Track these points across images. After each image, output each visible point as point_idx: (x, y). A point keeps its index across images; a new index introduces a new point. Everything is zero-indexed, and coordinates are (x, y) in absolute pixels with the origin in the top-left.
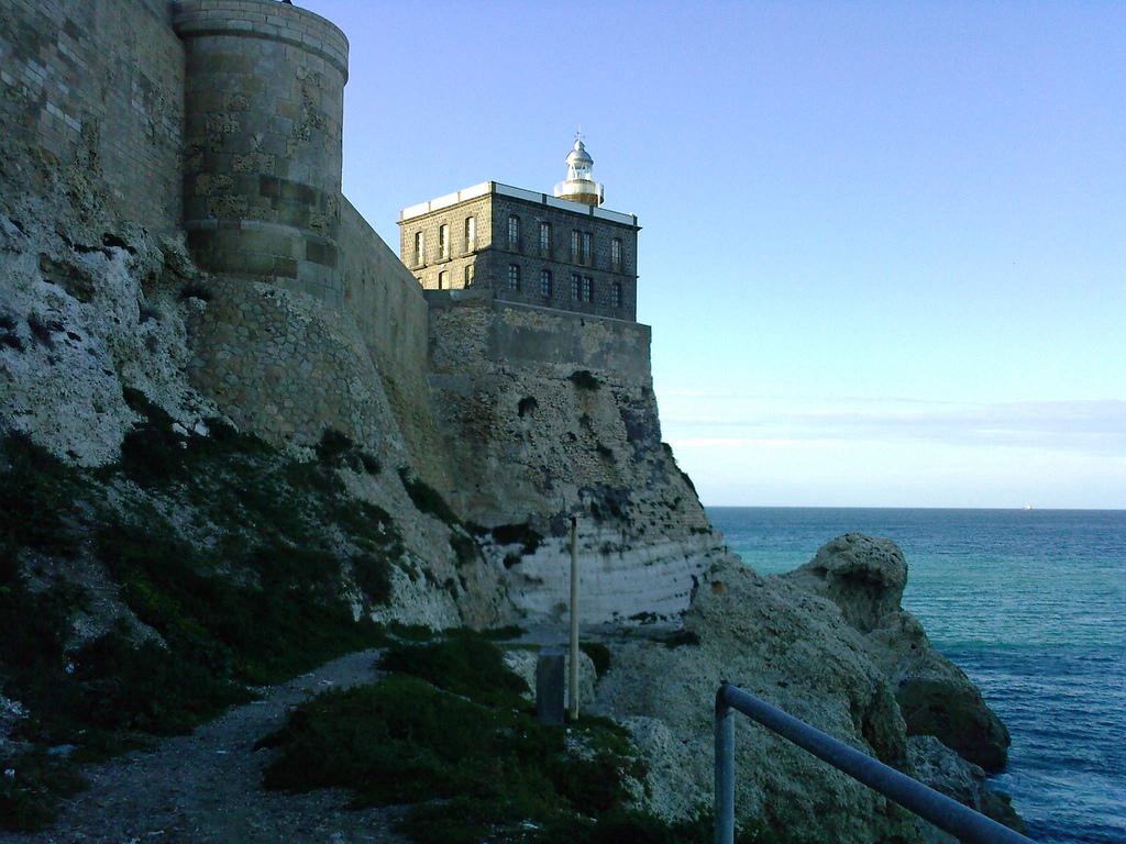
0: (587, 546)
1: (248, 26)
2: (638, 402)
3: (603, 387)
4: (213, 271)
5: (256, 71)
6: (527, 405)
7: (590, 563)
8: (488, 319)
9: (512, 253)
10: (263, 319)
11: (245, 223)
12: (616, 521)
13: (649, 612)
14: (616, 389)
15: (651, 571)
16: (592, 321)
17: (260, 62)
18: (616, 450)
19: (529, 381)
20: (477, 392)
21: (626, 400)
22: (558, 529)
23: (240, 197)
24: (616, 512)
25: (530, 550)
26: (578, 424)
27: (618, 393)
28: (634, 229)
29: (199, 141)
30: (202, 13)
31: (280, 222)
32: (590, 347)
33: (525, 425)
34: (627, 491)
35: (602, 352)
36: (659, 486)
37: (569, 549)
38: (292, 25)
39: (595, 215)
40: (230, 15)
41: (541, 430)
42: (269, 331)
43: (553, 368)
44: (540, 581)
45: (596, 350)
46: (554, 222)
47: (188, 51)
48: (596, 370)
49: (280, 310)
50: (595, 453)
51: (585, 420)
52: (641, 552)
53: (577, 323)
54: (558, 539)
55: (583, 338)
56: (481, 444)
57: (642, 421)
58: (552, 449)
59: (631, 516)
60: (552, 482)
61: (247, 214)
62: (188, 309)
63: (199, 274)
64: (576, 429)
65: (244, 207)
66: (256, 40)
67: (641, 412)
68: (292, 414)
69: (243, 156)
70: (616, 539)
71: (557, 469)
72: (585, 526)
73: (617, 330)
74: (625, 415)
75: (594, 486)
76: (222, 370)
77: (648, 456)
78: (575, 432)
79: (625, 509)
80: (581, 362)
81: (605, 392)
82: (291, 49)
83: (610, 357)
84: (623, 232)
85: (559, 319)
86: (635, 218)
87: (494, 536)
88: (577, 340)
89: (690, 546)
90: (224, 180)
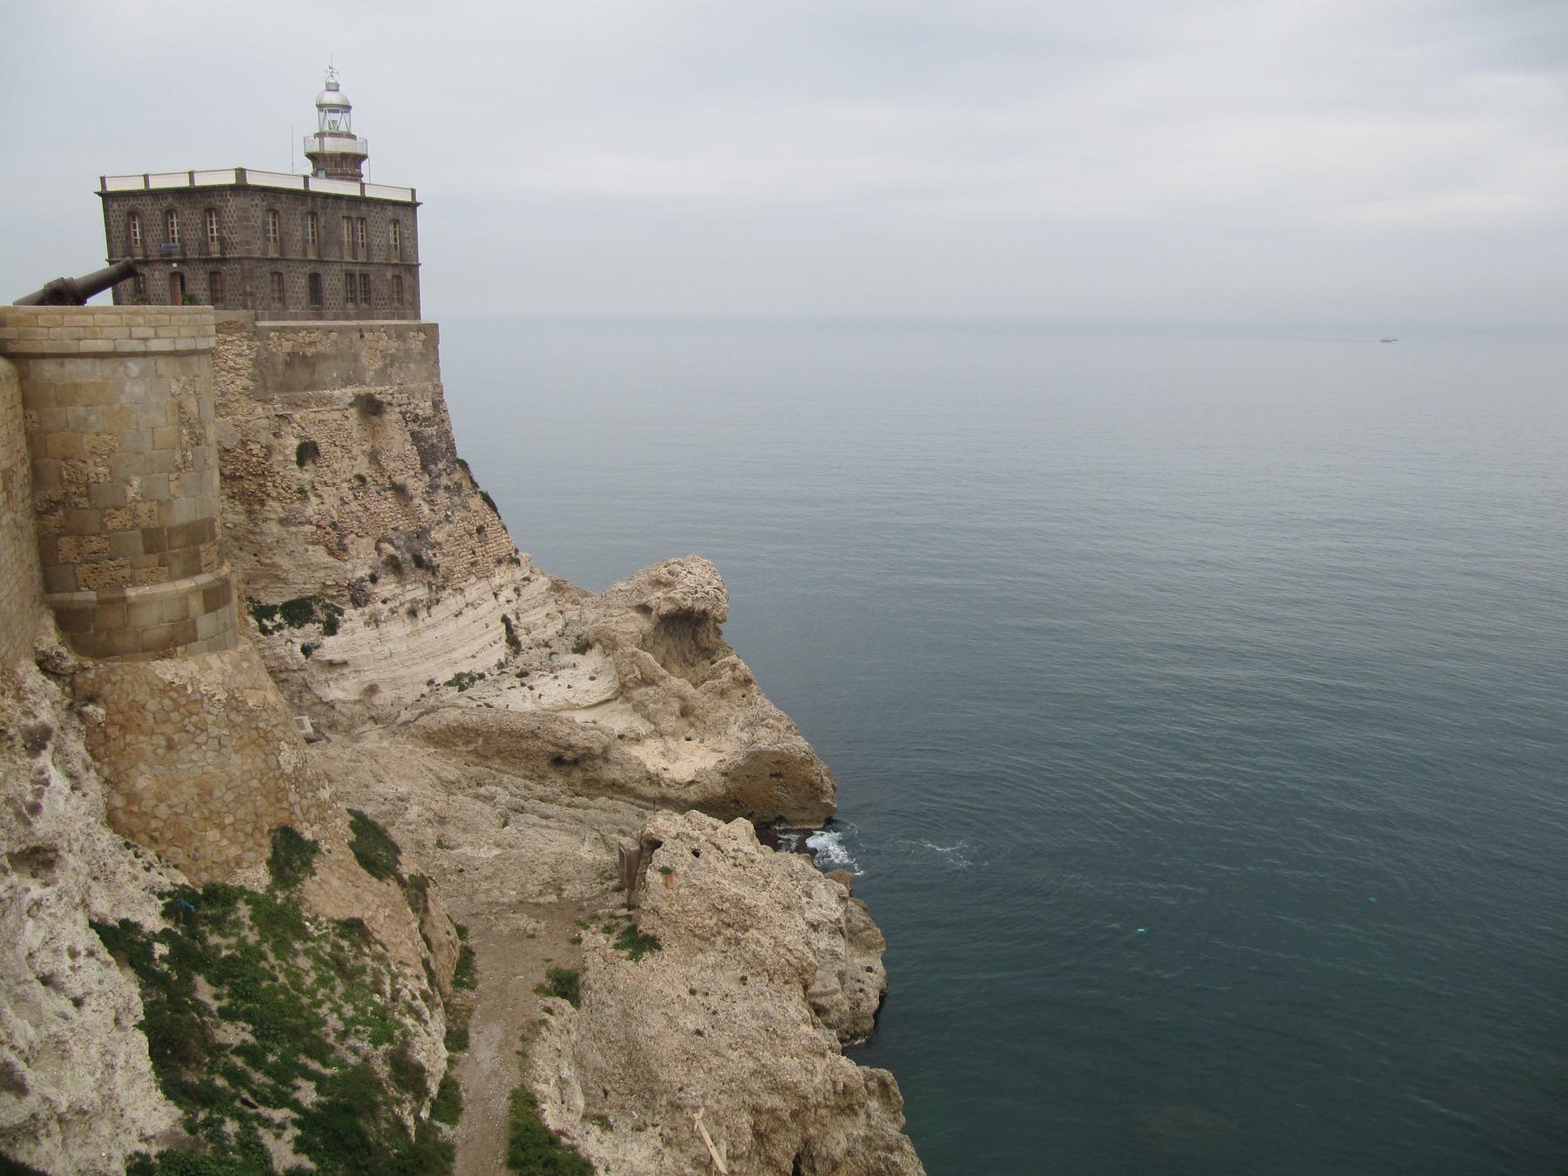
0: (393, 611)
1: (102, 345)
5: (123, 400)
6: (308, 452)
7: (397, 629)
8: (250, 348)
9: (272, 260)
10: (175, 716)
12: (420, 572)
13: (466, 671)
14: (403, 409)
15: (462, 621)
17: (127, 389)
19: (310, 421)
20: (244, 443)
21: (416, 419)
22: (359, 597)
23: (121, 561)
24: (419, 562)
25: (331, 628)
28: (412, 206)
29: (55, 493)
32: (371, 364)
33: (307, 475)
34: (422, 534)
35: (385, 366)
37: (374, 621)
38: (162, 332)
39: (367, 194)
44: (345, 663)
45: (378, 365)
46: (319, 211)
47: (23, 377)
48: (379, 389)
49: (193, 697)
50: (389, 494)
51: (374, 457)
52: (452, 602)
54: (360, 610)
56: (257, 507)
59: (436, 561)
62: (83, 722)
64: (363, 466)
65: (127, 572)
67: (430, 431)
68: (235, 830)
70: (421, 593)
72: (387, 587)
73: (401, 334)
74: (416, 438)
76: (149, 803)
79: (427, 554)
80: (362, 383)
81: (392, 415)
83: (394, 370)
84: (400, 212)
85: (334, 335)
86: (413, 191)
87: (284, 616)
88: (356, 358)
89: (497, 581)
90: (95, 544)
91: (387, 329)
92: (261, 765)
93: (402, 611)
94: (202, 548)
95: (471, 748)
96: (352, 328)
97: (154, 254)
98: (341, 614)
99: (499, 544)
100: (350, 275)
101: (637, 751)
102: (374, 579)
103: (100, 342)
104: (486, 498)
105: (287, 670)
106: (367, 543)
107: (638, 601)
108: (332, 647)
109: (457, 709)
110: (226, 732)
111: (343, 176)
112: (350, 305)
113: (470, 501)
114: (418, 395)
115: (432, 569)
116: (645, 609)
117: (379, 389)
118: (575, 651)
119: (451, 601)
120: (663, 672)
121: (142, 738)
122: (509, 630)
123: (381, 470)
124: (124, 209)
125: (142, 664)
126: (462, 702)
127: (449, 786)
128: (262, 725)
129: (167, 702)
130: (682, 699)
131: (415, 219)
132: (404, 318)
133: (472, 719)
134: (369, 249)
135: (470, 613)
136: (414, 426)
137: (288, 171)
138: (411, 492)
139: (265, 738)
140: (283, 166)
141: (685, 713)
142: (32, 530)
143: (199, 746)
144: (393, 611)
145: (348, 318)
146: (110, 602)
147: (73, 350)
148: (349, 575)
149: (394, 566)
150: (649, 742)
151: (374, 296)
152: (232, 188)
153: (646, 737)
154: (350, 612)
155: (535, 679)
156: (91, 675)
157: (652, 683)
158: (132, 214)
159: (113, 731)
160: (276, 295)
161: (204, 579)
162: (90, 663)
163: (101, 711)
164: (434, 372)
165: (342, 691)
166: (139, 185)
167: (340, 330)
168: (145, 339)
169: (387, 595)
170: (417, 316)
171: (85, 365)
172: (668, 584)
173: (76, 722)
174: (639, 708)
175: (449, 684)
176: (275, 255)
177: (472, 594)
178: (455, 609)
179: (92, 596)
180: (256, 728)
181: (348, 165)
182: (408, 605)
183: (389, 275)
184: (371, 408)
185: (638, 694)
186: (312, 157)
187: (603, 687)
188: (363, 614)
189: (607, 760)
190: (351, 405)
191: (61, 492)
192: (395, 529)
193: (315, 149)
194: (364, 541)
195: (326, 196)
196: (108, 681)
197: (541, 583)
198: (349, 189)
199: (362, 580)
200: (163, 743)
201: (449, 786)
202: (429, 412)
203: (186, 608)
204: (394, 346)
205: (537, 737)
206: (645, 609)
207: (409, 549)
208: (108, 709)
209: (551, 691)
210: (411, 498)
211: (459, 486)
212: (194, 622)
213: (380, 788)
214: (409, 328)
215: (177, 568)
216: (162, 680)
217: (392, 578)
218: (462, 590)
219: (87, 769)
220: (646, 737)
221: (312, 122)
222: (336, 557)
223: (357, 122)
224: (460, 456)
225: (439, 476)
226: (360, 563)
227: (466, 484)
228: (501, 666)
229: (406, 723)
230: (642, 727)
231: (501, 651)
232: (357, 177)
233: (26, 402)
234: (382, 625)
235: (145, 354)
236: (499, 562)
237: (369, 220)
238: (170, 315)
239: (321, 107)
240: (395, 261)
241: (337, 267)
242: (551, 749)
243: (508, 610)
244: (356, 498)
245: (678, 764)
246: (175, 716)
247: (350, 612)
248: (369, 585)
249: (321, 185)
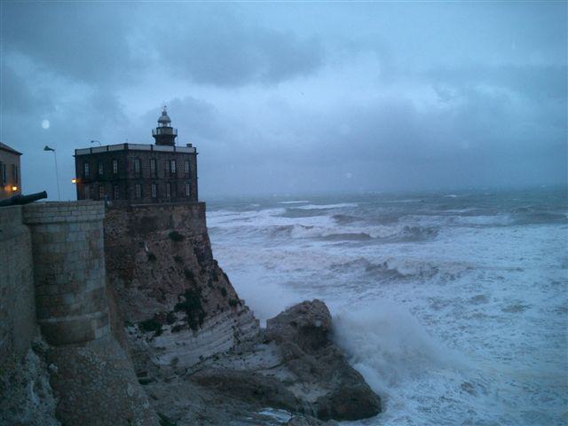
4: (57, 346)
6: (152, 257)
15: (215, 330)
22: (170, 320)
25: (159, 333)
32: (177, 220)
35: (184, 220)
44: (164, 348)
45: (180, 220)
51: (178, 259)
60: (166, 295)
64: (173, 264)
74: (196, 250)
95: (218, 386)
101: (291, 389)
105: (141, 351)
107: (291, 320)
108: (159, 341)
109: (213, 369)
116: (294, 324)
118: (264, 343)
120: (303, 353)
126: (214, 366)
127: (207, 403)
130: (312, 365)
141: (312, 371)
142: (32, 293)
143: (94, 383)
150: (297, 385)
152: (123, 151)
153: (295, 382)
157: (298, 357)
165: (164, 361)
172: (304, 313)
173: (46, 373)
174: (291, 369)
185: (291, 362)
186: (154, 136)
187: (275, 361)
189: (277, 393)
195: (160, 152)
198: (170, 149)
200: (80, 382)
201: (207, 403)
205: (246, 383)
206: (294, 324)
209: (253, 361)
213: (177, 403)
219: (49, 392)
220: (295, 382)
229: (190, 375)
230: (292, 377)
232: (172, 144)
239: (159, 122)
242: (253, 387)
245: (309, 395)
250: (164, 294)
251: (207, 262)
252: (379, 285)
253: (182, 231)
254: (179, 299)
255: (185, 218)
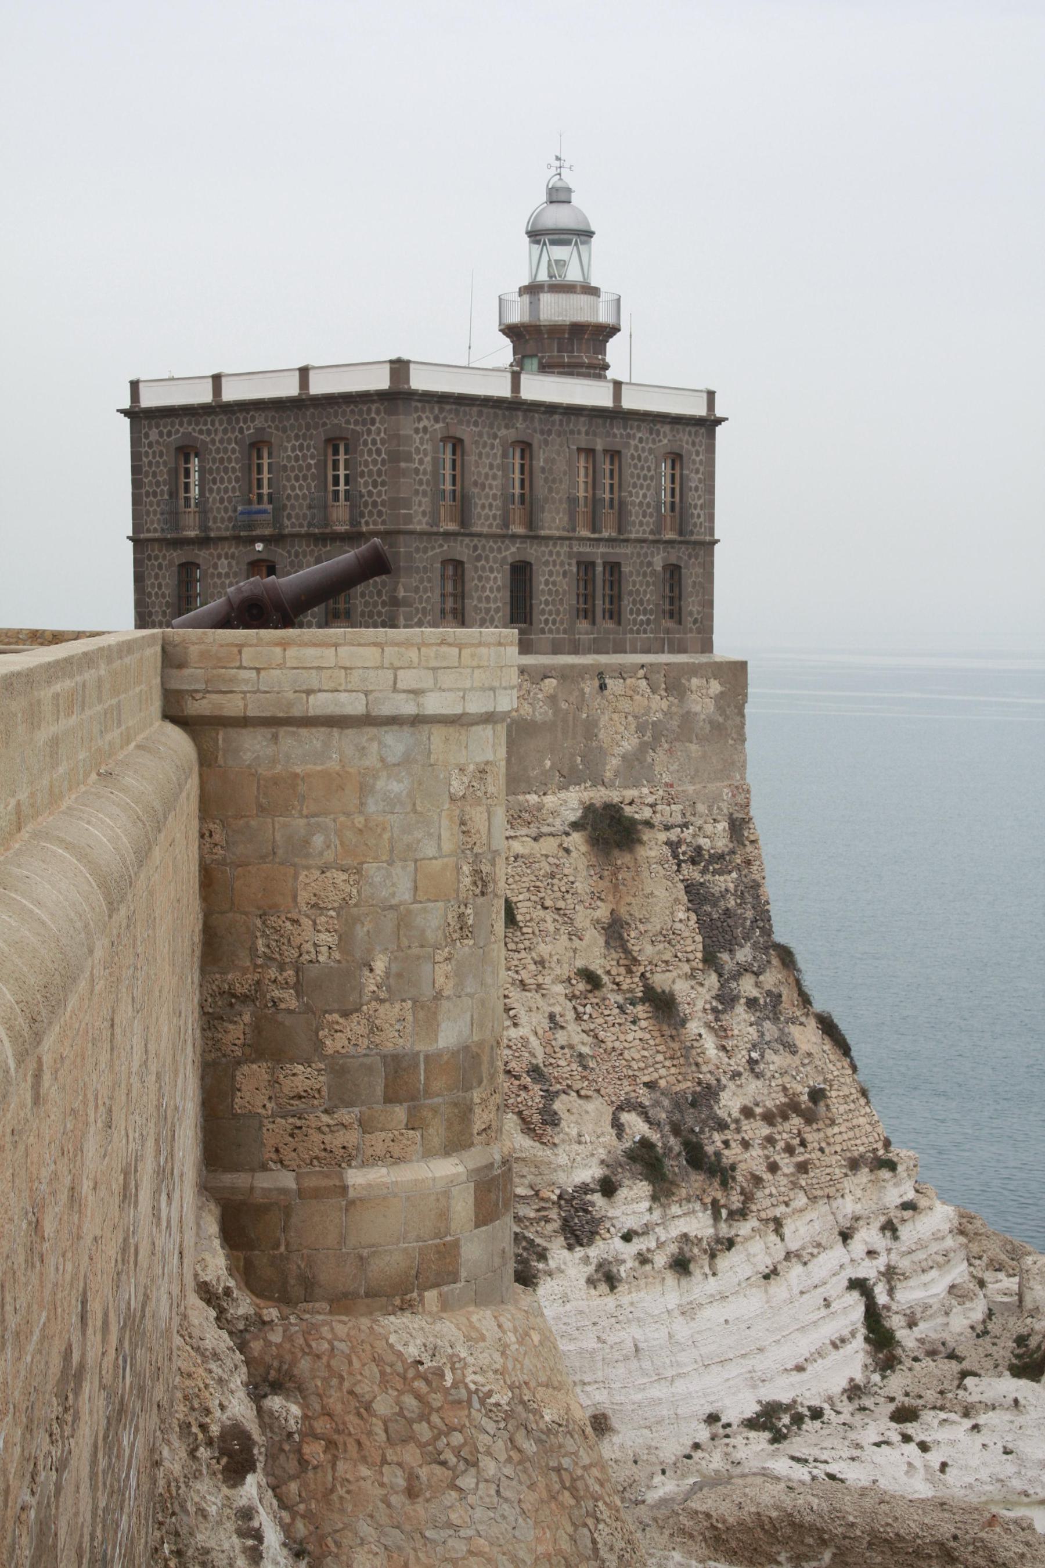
0: (643, 1259)
1: (353, 705)
2: (721, 857)
3: (646, 835)
4: (285, 1299)
9: (447, 535)
10: (423, 1430)
11: (356, 1178)
12: (697, 1180)
13: (785, 1398)
14: (673, 835)
15: (778, 1289)
16: (621, 673)
17: (380, 784)
18: (681, 988)
21: (697, 856)
24: (696, 1157)
26: (601, 941)
27: (679, 843)
28: (709, 424)
30: (244, 674)
31: (428, 1154)
32: (620, 740)
34: (709, 1093)
35: (643, 747)
36: (776, 1060)
37: (607, 1277)
38: (447, 679)
40: (313, 680)
41: (524, 975)
42: (444, 1463)
43: (540, 807)
45: (629, 744)
47: (206, 760)
48: (630, 793)
50: (641, 1011)
51: (615, 931)
52: (756, 1250)
53: (589, 686)
54: (579, 1252)
55: (604, 720)
57: (732, 903)
58: (552, 1017)
60: (557, 1106)
61: (348, 1157)
63: (259, 1315)
64: (595, 955)
65: (351, 1137)
66: (372, 731)
67: (725, 882)
69: (346, 1014)
70: (699, 1224)
71: (565, 1067)
72: (633, 1204)
73: (674, 684)
74: (697, 896)
75: (645, 1097)
77: (747, 986)
78: (597, 966)
80: (599, 781)
81: (653, 847)
82: (438, 734)
83: (659, 756)
84: (684, 439)
85: (550, 684)
86: (711, 395)
88: (590, 729)
89: (848, 1206)
91: (649, 672)
92: (565, 1545)
93: (661, 1260)
94: (476, 1095)
96: (582, 672)
97: (219, 527)
98: (542, 1256)
99: (852, 1127)
100: (586, 566)
102: (608, 1188)
103: (343, 696)
104: (828, 1027)
106: (598, 1111)
110: (508, 1471)
111: (572, 369)
112: (583, 625)
113: (795, 1030)
114: (701, 808)
115: (720, 1172)
117: (630, 793)
118: (1019, 1371)
119: (756, 1246)
121: (364, 1471)
122: (873, 1317)
123: (631, 962)
124: (171, 439)
125: (365, 1322)
126: (781, 1466)
128: (566, 1462)
129: (409, 1401)
131: (711, 449)
132: (680, 648)
133: (809, 1504)
134: (621, 510)
135: (795, 1272)
136: (692, 872)
137: (465, 364)
138: (684, 1009)
139: (573, 1490)
140: (466, 352)
144: (643, 1259)
145: (575, 651)
146: (317, 1194)
147: (296, 712)
148: (562, 1178)
149: (645, 1160)
151: (627, 603)
152: (381, 396)
154: (559, 1254)
155: (929, 1426)
156: (276, 1337)
158: (185, 451)
159: (314, 1451)
160: (450, 603)
161: (475, 1157)
162: (272, 1313)
163: (295, 1410)
164: (733, 764)
166: (204, 396)
167: (566, 675)
168: (416, 692)
169: (631, 1223)
170: (707, 646)
171: (314, 738)
175: (751, 1424)
176: (452, 527)
177: (799, 1231)
178: (764, 1263)
179: (287, 1180)
180: (558, 1470)
181: (580, 345)
182: (673, 1248)
183: (658, 562)
184: (611, 832)
186: (511, 331)
188: (586, 1260)
190: (575, 826)
191: (252, 977)
192: (650, 1085)
193: (516, 316)
194: (590, 1106)
195: (551, 409)
196: (308, 1350)
197: (939, 1217)
198: (591, 394)
199: (585, 1189)
200: (401, 1482)
202: (722, 844)
203: (444, 1215)
204: (659, 704)
207: (676, 1131)
208: (305, 1406)
210: (683, 1022)
211: (776, 998)
212: (456, 1244)
214: (694, 670)
215: (437, 1132)
216: (399, 1355)
217: (643, 1188)
218: (778, 1224)
221: (519, 263)
222: (539, 1138)
223: (604, 265)
224: (780, 936)
225: (736, 976)
226: (578, 1157)
227: (788, 994)
228: (854, 1391)
231: (854, 1361)
232: (598, 370)
233: (209, 806)
234: (622, 1288)
235: (417, 721)
236: (854, 1165)
237: (628, 453)
238: (461, 647)
239: (535, 235)
240: (670, 536)
241: (563, 549)
243: (868, 1270)
244: (579, 1017)
246: (423, 1430)
247: (559, 1254)
248: (597, 1198)
249: (542, 388)
250: (550, 1096)
251: (744, 954)
252: (22, 1204)
253: (637, 800)
254: (618, 1126)
255: (653, 735)
